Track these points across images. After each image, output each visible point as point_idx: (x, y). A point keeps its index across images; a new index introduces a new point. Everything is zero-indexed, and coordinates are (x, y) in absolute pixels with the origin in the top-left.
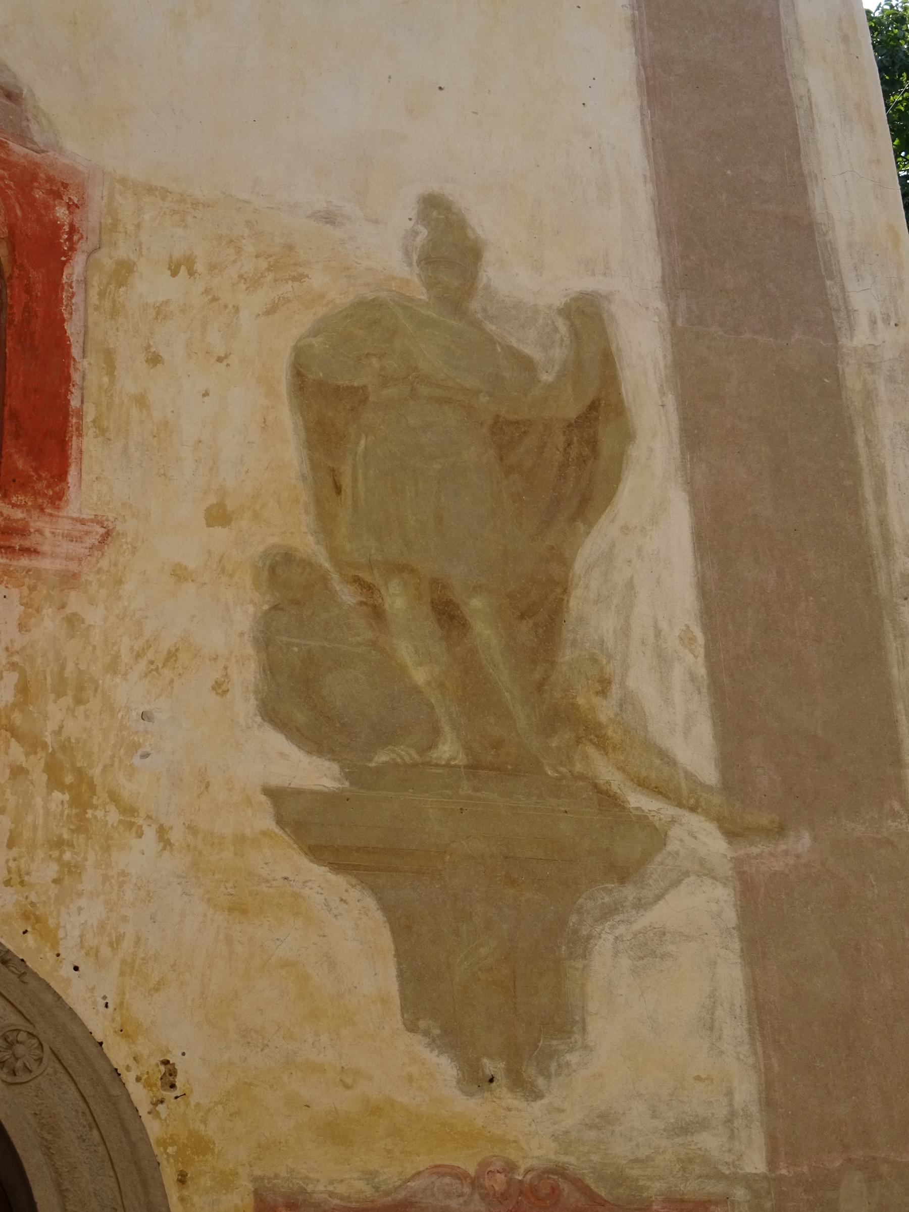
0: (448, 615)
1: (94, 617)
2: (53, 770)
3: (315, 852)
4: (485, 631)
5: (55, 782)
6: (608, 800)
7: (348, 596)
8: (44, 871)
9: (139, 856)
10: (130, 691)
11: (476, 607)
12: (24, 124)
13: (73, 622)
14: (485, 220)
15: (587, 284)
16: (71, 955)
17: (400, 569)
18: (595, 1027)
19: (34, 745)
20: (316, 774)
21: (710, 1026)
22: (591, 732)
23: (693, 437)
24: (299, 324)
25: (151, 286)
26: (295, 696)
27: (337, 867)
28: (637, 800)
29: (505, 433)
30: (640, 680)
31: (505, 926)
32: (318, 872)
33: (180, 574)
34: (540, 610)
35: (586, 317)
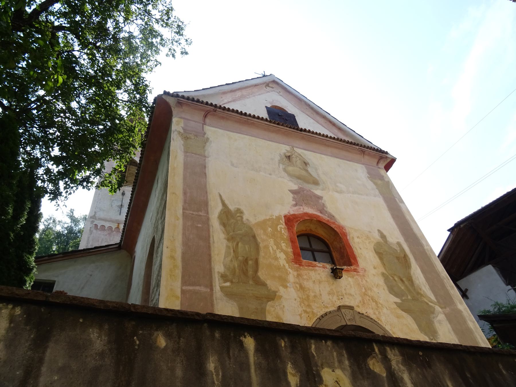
0: (402, 280)
1: (368, 280)
2: (372, 299)
3: (403, 310)
4: (406, 282)
5: (373, 301)
6: (427, 304)
7: (391, 278)
8: (377, 313)
9: (385, 310)
10: (375, 289)
11: (404, 279)
12: (274, 217)
13: (366, 281)
14: (385, 233)
15: (397, 240)
16: (384, 324)
17: (395, 275)
18: (439, 332)
19: (369, 297)
20: (398, 300)
21: (450, 332)
22: (422, 295)
23: (416, 259)
24: (373, 245)
25: (356, 240)
26: (392, 290)
27: (405, 312)
28: (430, 304)
29: (398, 258)
30: (423, 288)
31: (97, 147)
32: (403, 313)
33: (374, 275)
34: (410, 279)
35: (399, 244)
